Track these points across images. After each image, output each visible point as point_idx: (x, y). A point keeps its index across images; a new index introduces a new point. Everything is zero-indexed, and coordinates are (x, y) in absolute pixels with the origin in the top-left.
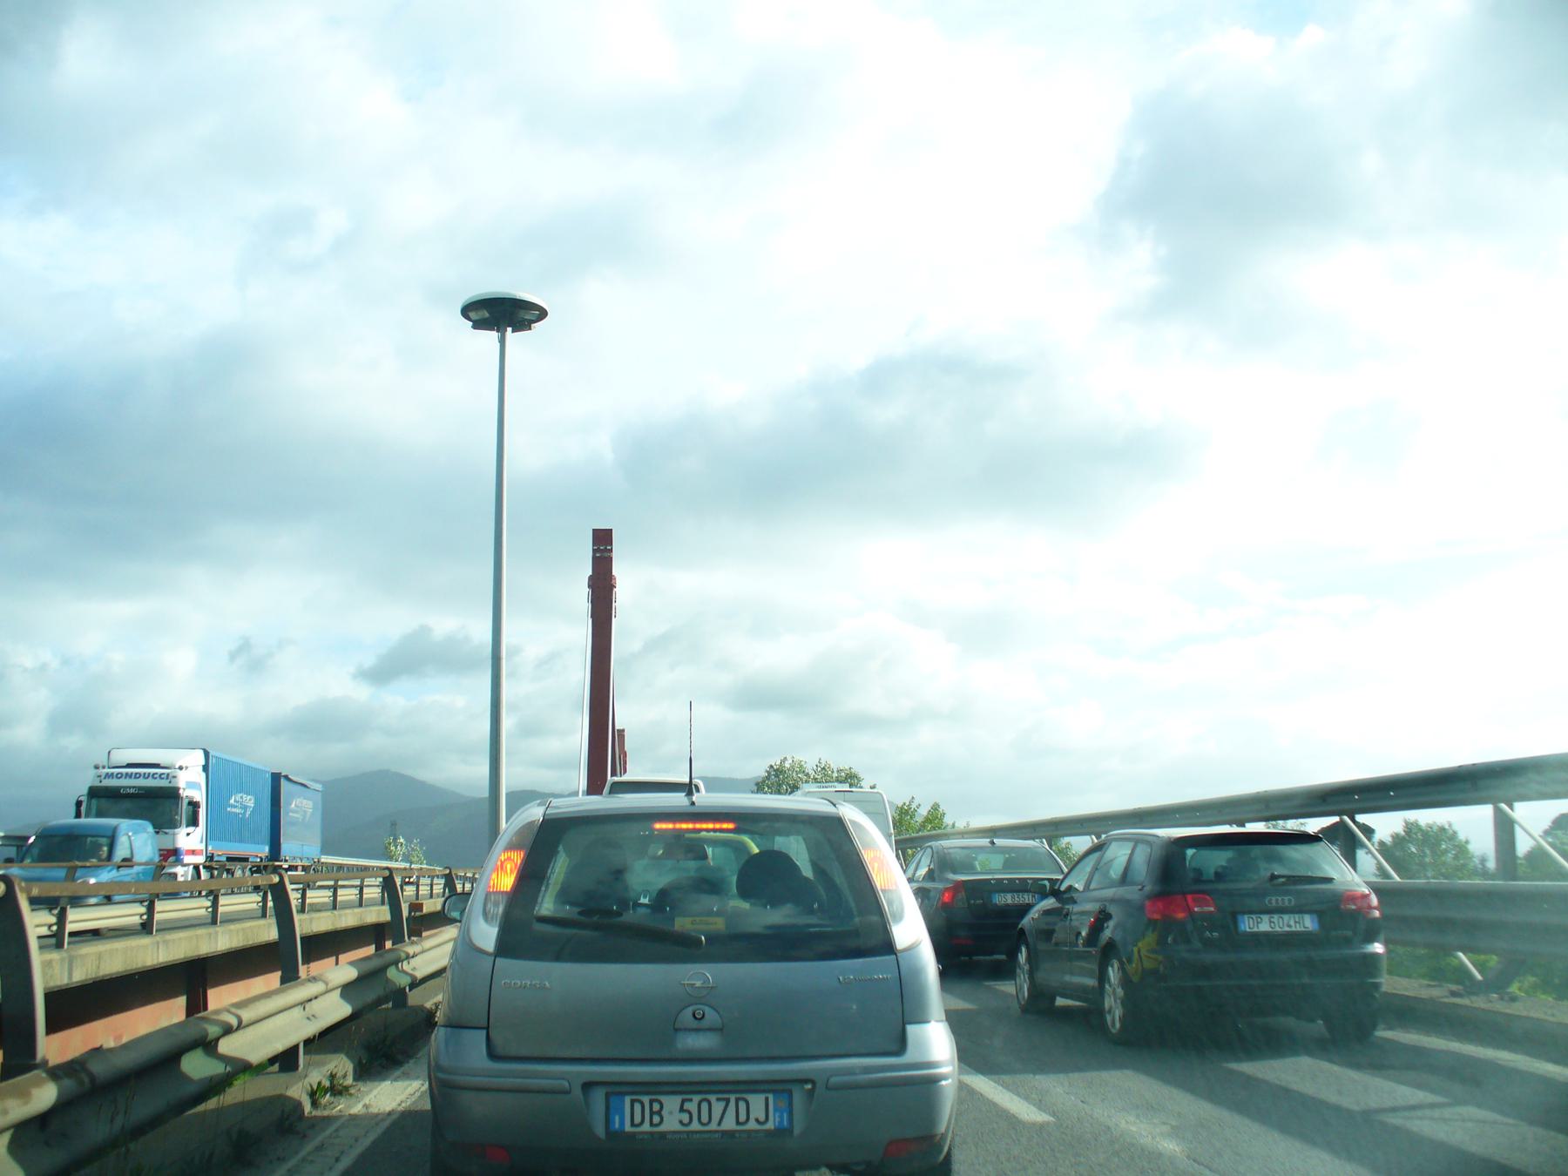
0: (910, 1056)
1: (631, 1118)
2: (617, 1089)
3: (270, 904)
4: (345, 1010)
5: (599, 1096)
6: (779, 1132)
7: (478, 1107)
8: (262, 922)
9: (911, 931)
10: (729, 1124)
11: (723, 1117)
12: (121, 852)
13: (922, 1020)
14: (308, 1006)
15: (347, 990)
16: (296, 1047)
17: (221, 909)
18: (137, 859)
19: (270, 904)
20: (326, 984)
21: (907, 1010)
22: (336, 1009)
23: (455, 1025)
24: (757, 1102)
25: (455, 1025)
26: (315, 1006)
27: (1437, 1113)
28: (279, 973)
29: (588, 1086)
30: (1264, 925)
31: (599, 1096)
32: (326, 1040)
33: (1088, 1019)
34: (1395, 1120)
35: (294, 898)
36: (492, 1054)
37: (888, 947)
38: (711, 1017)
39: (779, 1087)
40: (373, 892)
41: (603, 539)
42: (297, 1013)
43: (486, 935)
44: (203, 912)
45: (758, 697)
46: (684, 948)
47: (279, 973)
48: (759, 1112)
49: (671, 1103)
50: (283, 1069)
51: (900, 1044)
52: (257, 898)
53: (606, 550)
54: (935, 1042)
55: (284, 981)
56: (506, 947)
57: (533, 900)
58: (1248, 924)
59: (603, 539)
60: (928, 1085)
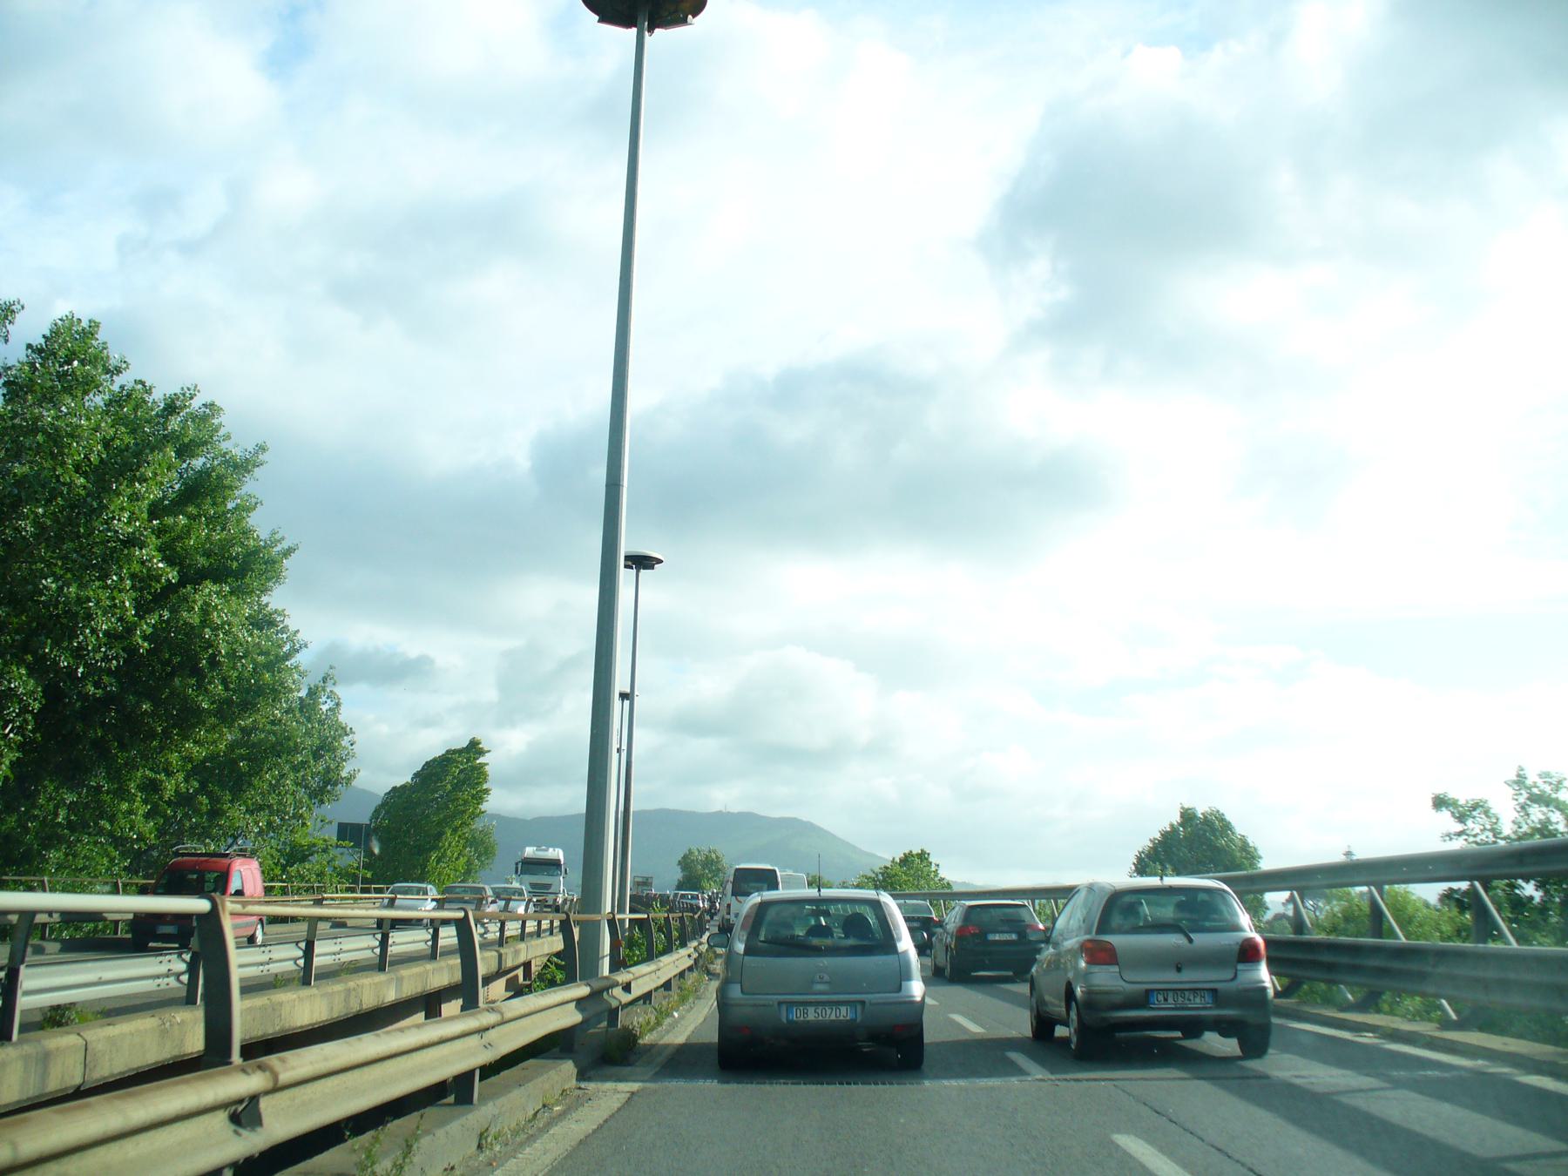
0: (903, 993)
1: (797, 1015)
2: (791, 1004)
4: (577, 1018)
5: (784, 1008)
9: (906, 944)
10: (833, 1017)
11: (831, 1015)
12: (234, 885)
15: (580, 1003)
18: (247, 892)
20: (275, 1076)
21: (904, 974)
22: (571, 1017)
24: (843, 1009)
26: (492, 1034)
27: (1381, 1093)
28: (460, 1001)
29: (780, 1003)
30: (997, 937)
31: (784, 1008)
34: (1345, 1099)
35: (477, 932)
38: (826, 978)
42: (474, 1041)
43: (740, 947)
44: (422, 946)
46: (817, 951)
47: (460, 1001)
48: (844, 1014)
49: (811, 1010)
51: (899, 989)
54: (917, 988)
55: (463, 1008)
56: (748, 951)
58: (991, 937)
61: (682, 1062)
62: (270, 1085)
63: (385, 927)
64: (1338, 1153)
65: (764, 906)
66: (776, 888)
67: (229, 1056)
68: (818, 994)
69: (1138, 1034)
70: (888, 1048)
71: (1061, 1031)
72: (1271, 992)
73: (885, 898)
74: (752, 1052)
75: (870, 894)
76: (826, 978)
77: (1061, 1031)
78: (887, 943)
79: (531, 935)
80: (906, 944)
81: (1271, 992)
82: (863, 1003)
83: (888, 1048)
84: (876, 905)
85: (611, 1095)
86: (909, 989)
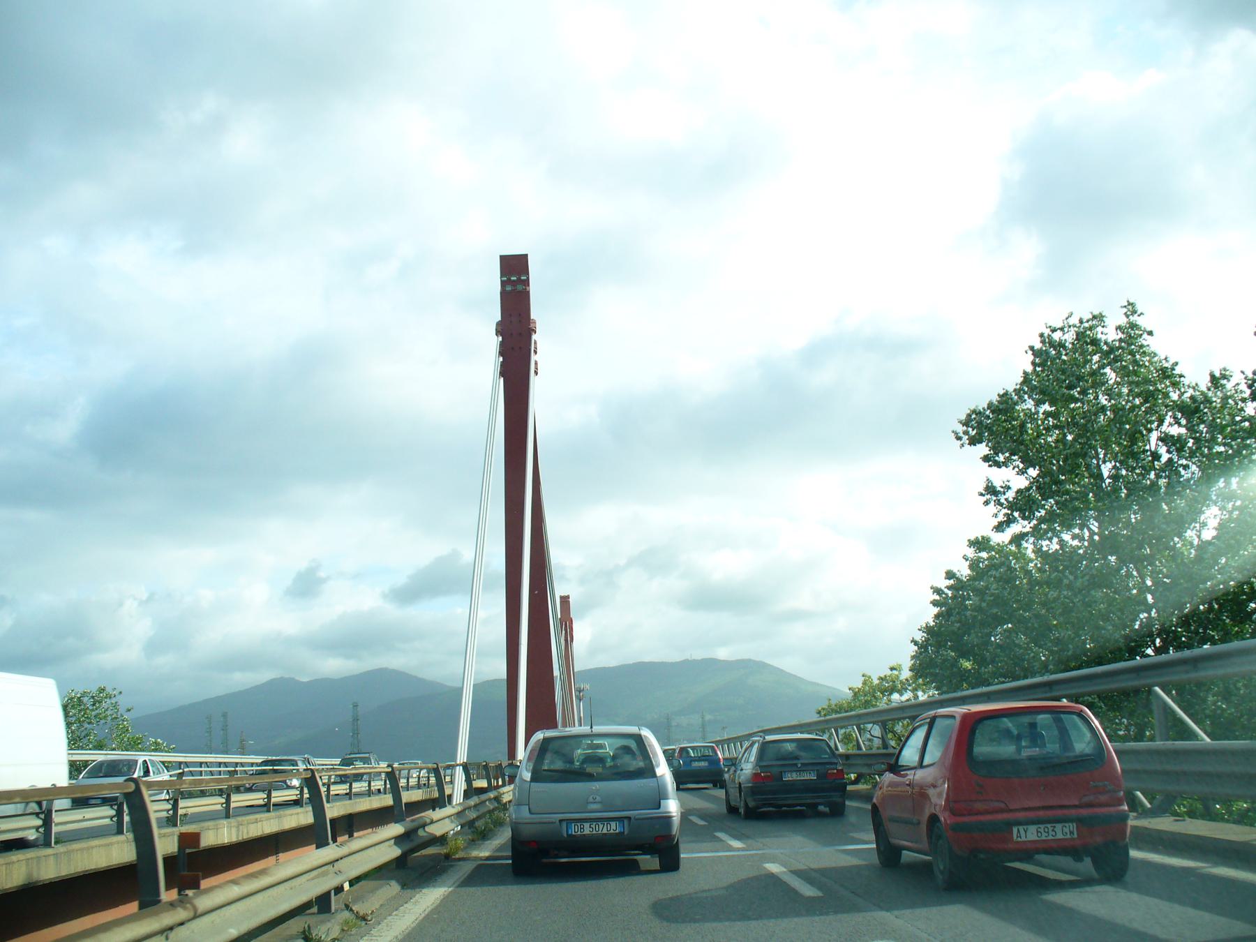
1: (574, 830)
3: (126, 818)
4: (396, 852)
5: (564, 825)
6: (621, 833)
7: (527, 831)
8: (120, 838)
9: (663, 770)
10: (605, 831)
11: (603, 829)
13: (666, 798)
14: (172, 935)
15: (399, 840)
16: (328, 893)
17: (233, 805)
19: (126, 818)
21: (661, 795)
23: (519, 804)
24: (613, 824)
25: (519, 804)
29: (561, 821)
31: (564, 825)
32: (380, 873)
33: (921, 871)
36: (531, 812)
37: (654, 775)
39: (619, 819)
40: (378, 784)
41: (514, 270)
44: (219, 807)
45: (708, 598)
46: (590, 777)
48: (614, 828)
49: (587, 825)
50: (320, 912)
51: (659, 807)
52: (109, 811)
53: (520, 281)
56: (534, 779)
57: (542, 763)
59: (514, 270)
60: (667, 819)
61: (484, 874)
62: (191, 914)
63: (349, 795)
64: (834, 865)
65: (546, 741)
66: (555, 726)
67: (158, 894)
68: (588, 807)
69: (1112, 809)
70: (654, 847)
71: (907, 856)
72: (676, 820)
73: (646, 733)
74: (541, 858)
75: (632, 729)
76: (598, 799)
77: (907, 856)
78: (648, 771)
79: (413, 787)
80: (663, 770)
81: (676, 820)
82: (629, 818)
83: (654, 847)
84: (639, 739)
85: (431, 897)
86: (666, 807)
